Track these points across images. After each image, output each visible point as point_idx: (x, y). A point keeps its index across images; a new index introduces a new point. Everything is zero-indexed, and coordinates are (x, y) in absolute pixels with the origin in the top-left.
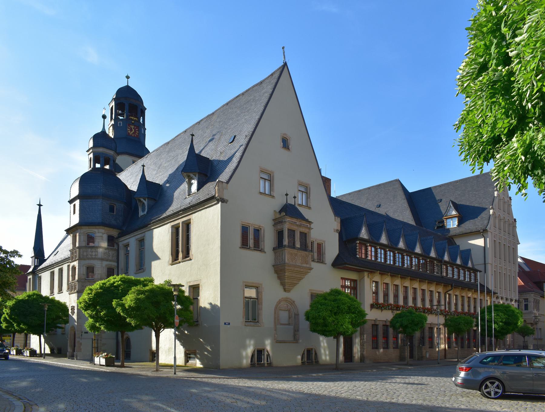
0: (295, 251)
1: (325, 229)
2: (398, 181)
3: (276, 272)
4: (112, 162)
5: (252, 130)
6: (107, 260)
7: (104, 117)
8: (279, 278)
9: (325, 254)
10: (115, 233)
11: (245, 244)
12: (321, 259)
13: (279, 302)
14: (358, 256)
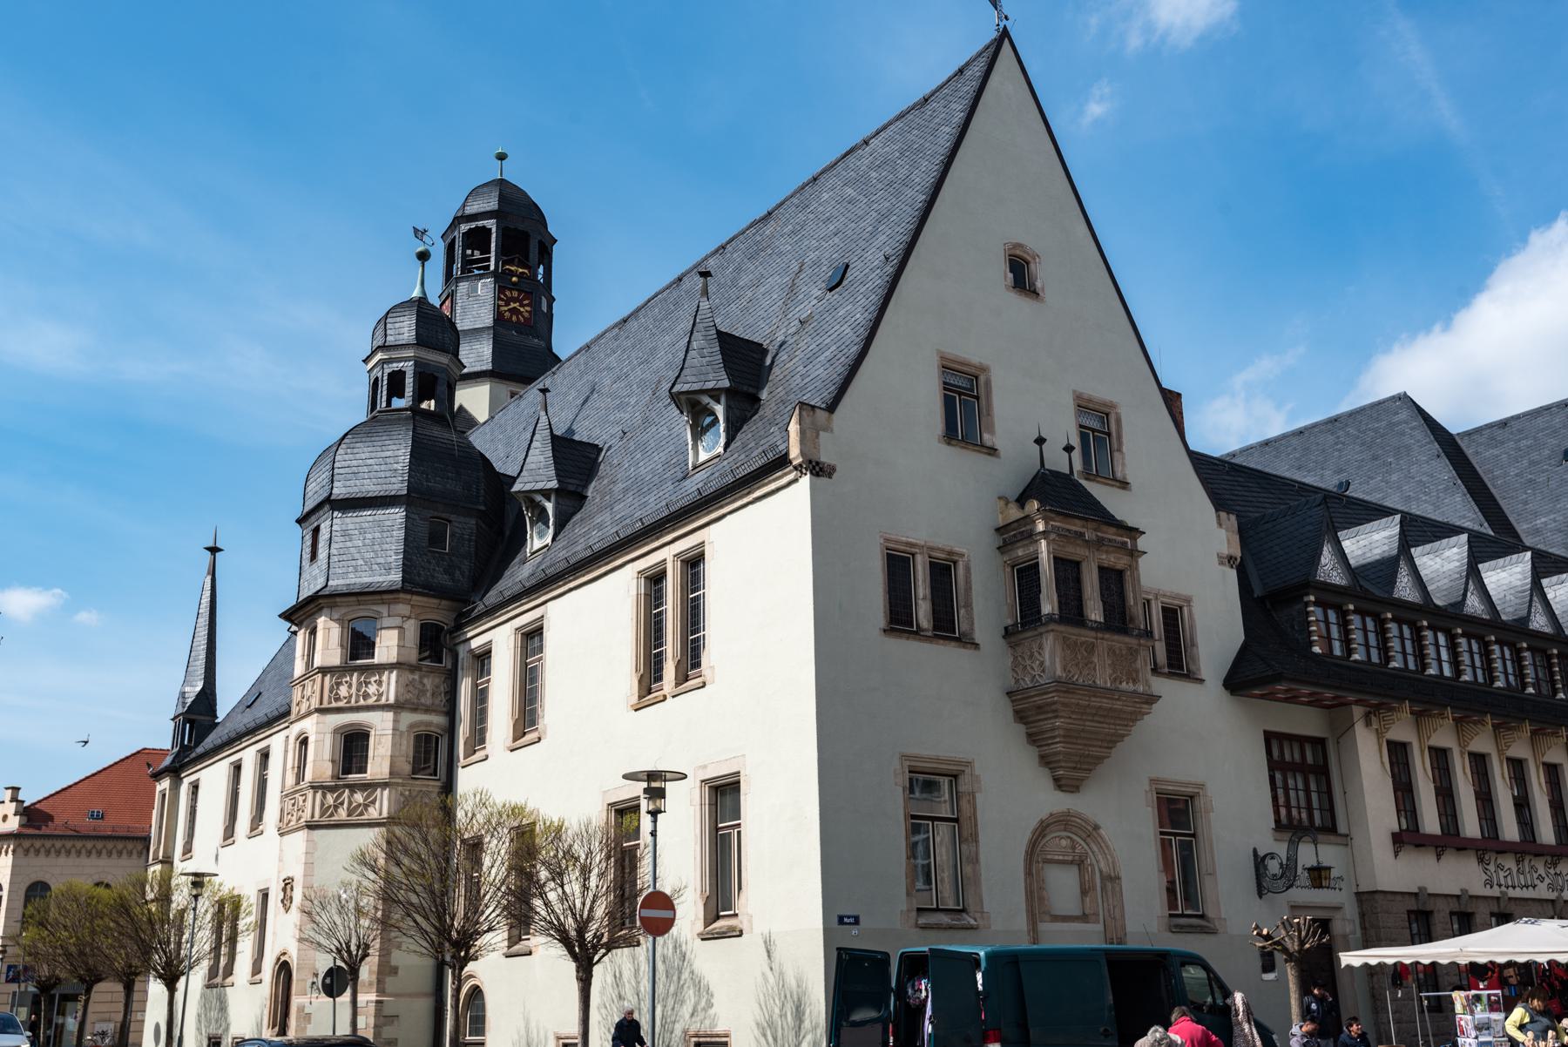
0: (1087, 636)
1: (1188, 559)
2: (1404, 399)
3: (1020, 716)
4: (441, 389)
5: (907, 238)
6: (415, 710)
7: (423, 256)
8: (1033, 738)
9: (1193, 644)
10: (438, 611)
11: (899, 619)
12: (1178, 664)
13: (1042, 830)
14: (1317, 649)
